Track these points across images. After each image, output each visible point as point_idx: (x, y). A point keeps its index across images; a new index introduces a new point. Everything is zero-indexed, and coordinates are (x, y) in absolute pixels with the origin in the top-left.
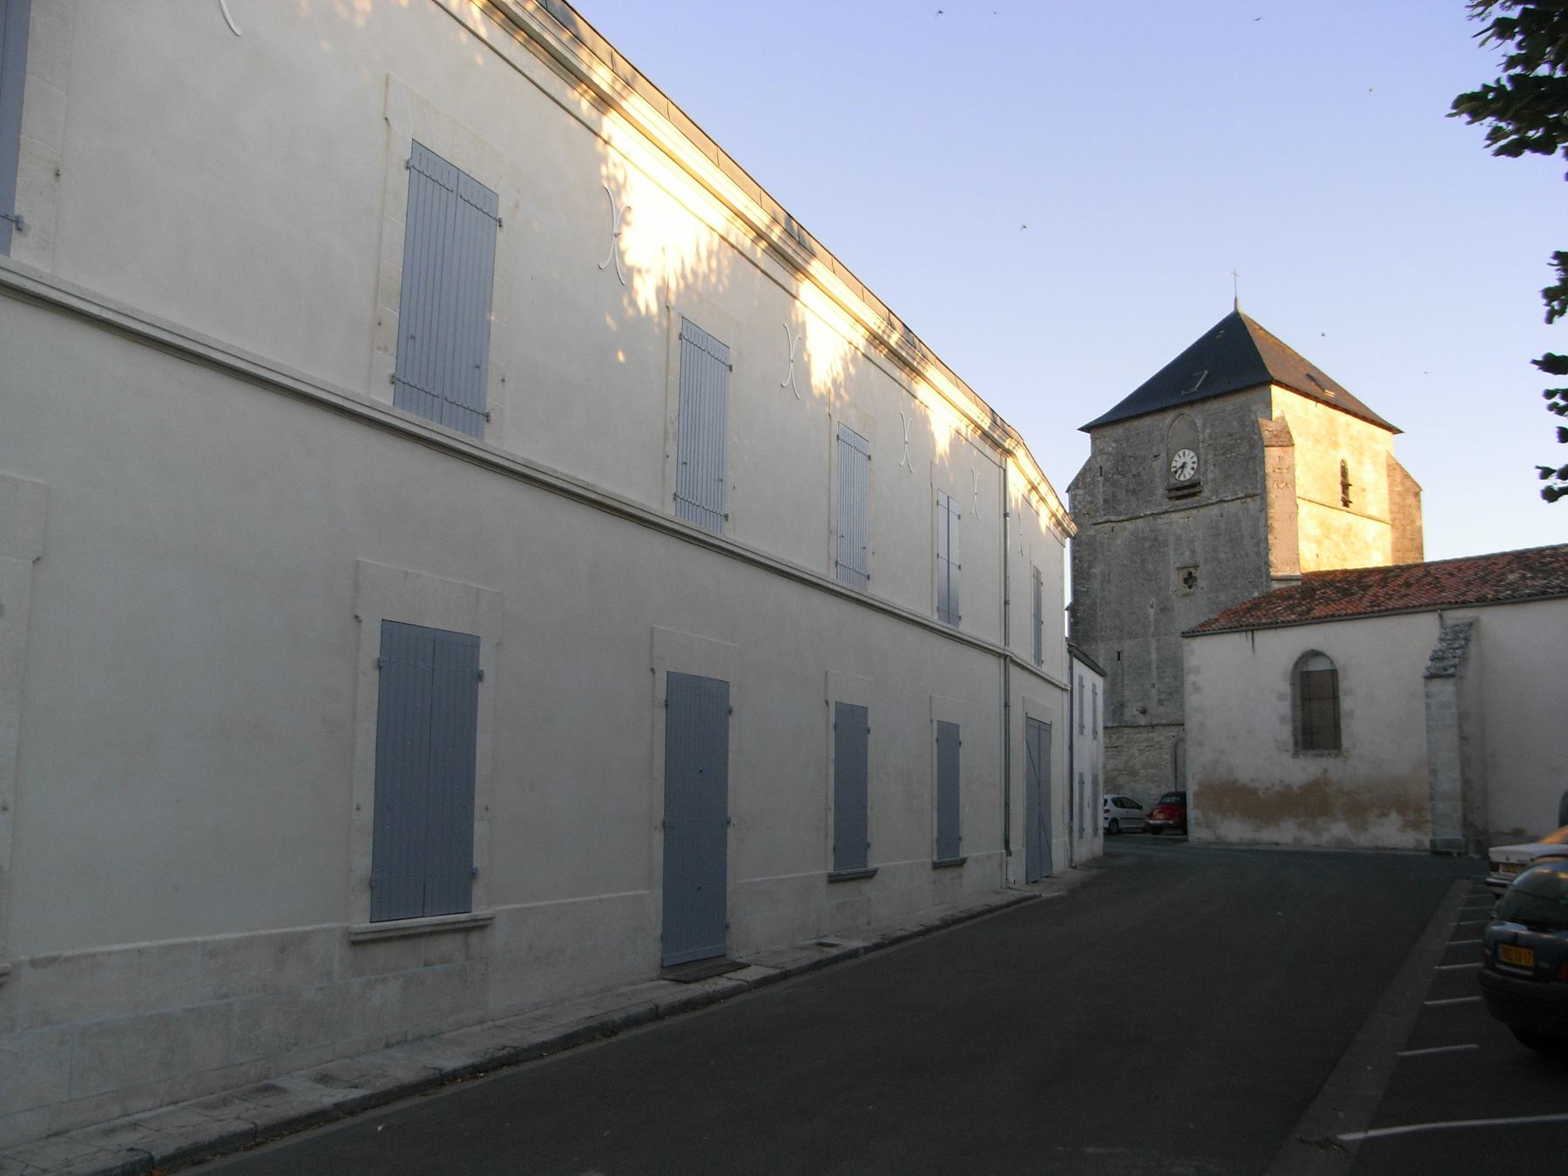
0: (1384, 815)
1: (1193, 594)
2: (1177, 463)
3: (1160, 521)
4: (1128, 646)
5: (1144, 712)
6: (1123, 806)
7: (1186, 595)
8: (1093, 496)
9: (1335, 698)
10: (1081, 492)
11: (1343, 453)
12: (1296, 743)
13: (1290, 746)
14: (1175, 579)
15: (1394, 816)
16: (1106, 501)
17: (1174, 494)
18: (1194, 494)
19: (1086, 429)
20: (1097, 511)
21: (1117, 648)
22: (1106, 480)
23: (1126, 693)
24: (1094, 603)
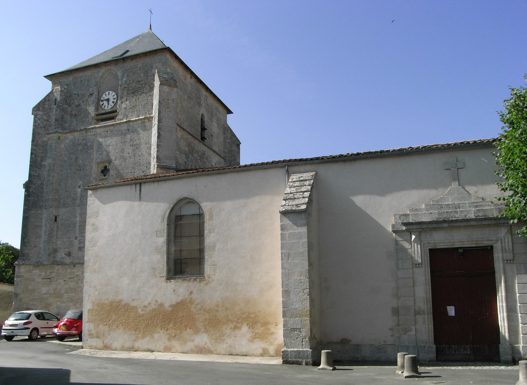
0: (236, 328)
1: (106, 179)
2: (104, 97)
3: (89, 134)
4: (62, 212)
5: (69, 254)
6: (44, 319)
7: (103, 180)
8: (49, 116)
9: (201, 235)
10: (41, 113)
11: (203, 111)
12: (169, 271)
13: (165, 274)
14: (95, 170)
15: (245, 328)
16: (56, 120)
17: (100, 117)
18: (113, 118)
19: (49, 77)
20: (50, 126)
21: (55, 213)
22: (58, 107)
23: (59, 242)
24: (42, 184)
